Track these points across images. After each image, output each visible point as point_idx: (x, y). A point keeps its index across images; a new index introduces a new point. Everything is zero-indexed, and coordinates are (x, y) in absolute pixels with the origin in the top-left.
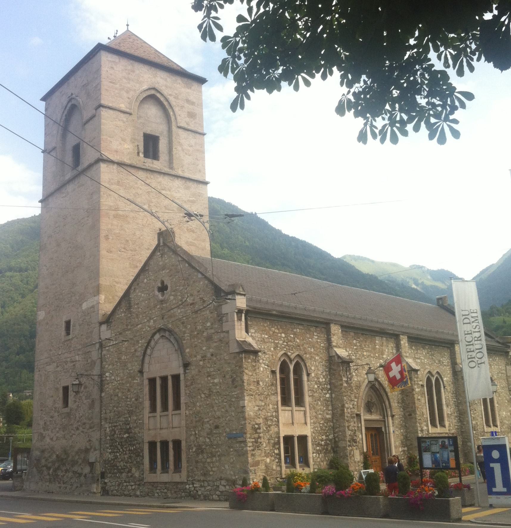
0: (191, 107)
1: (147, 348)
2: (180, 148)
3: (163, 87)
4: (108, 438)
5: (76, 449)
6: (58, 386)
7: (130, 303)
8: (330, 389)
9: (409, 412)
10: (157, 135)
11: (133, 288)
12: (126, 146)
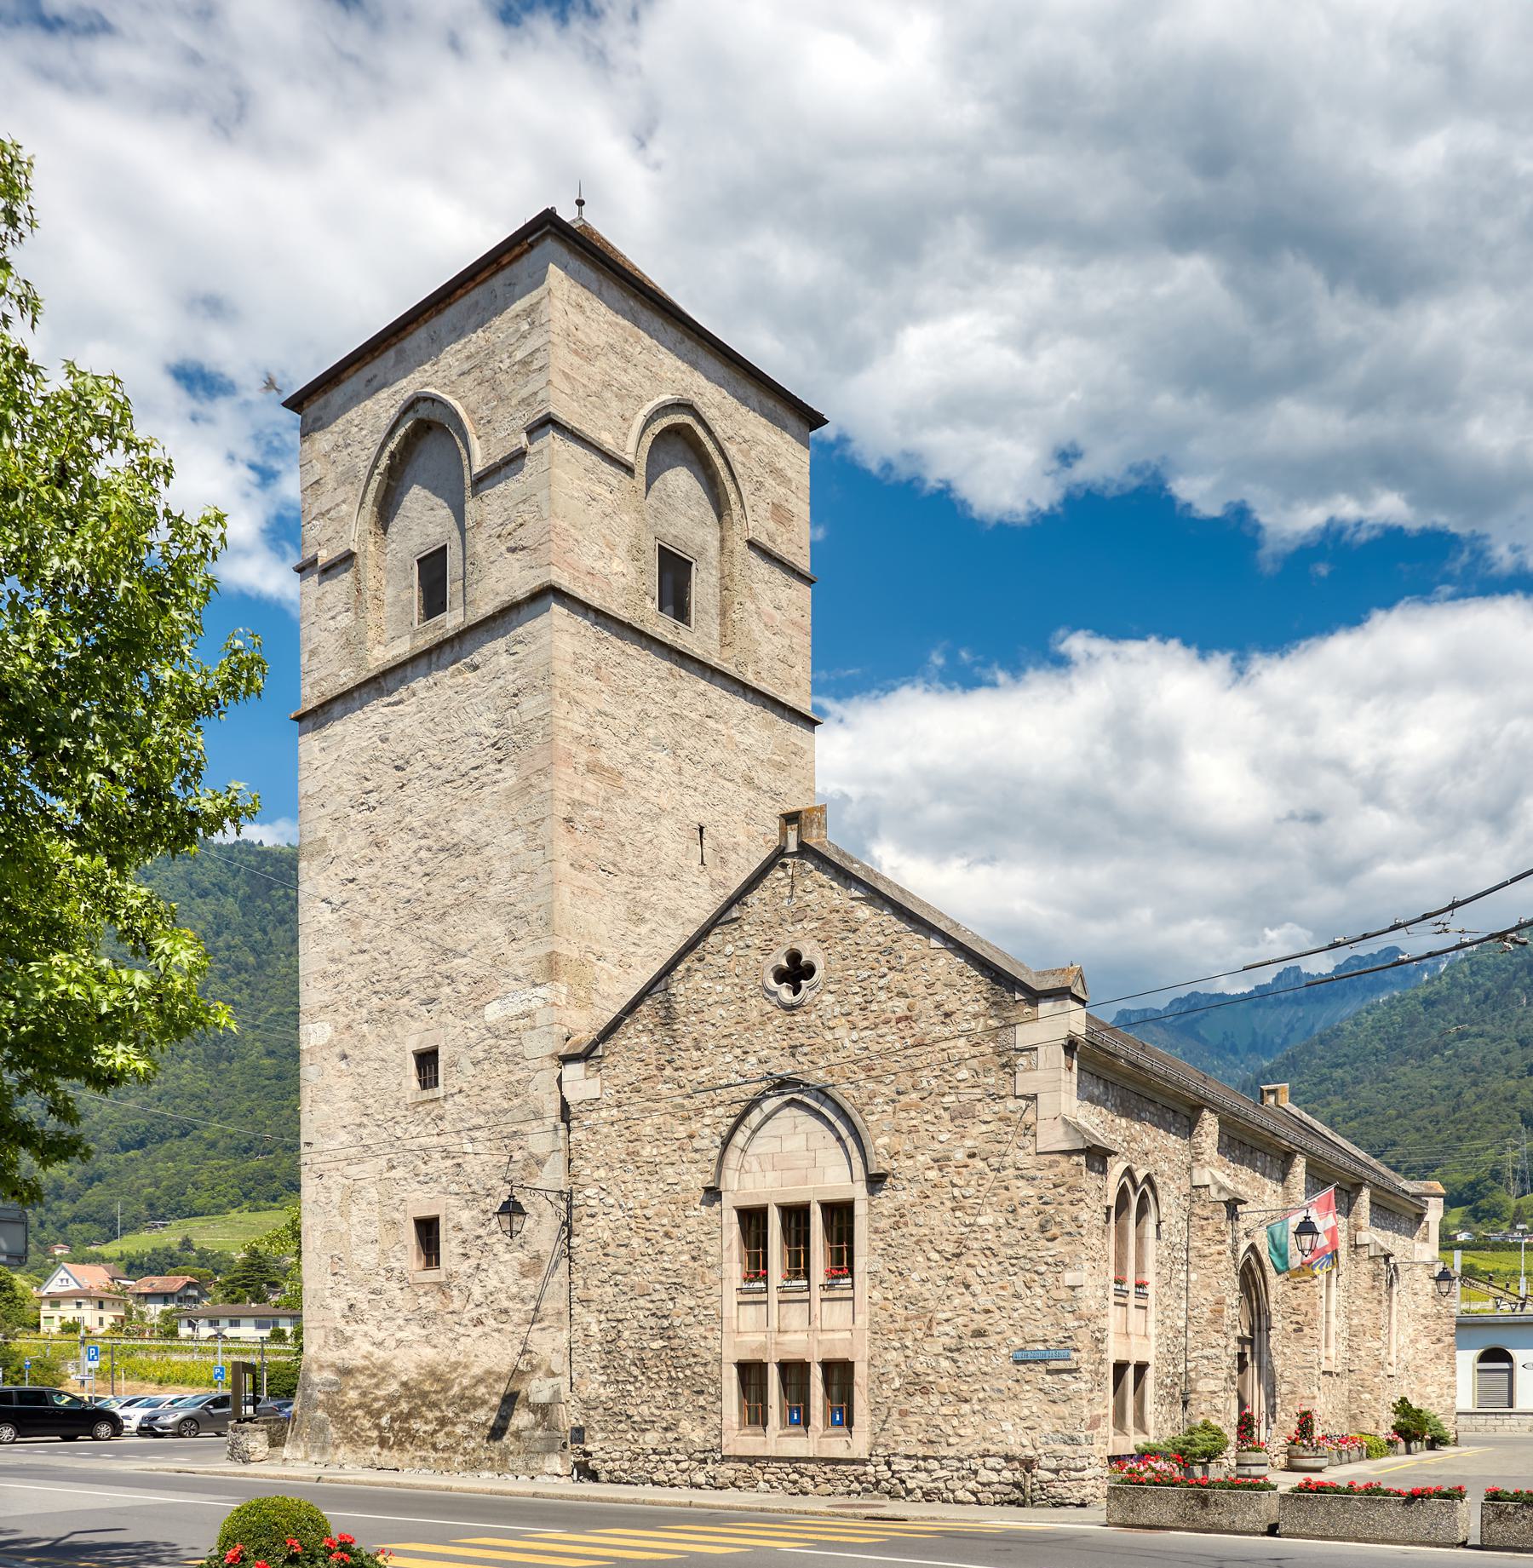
0: (782, 490)
1: (734, 1129)
4: (596, 1347)
5: (477, 1370)
6: (397, 1216)
12: (617, 566)
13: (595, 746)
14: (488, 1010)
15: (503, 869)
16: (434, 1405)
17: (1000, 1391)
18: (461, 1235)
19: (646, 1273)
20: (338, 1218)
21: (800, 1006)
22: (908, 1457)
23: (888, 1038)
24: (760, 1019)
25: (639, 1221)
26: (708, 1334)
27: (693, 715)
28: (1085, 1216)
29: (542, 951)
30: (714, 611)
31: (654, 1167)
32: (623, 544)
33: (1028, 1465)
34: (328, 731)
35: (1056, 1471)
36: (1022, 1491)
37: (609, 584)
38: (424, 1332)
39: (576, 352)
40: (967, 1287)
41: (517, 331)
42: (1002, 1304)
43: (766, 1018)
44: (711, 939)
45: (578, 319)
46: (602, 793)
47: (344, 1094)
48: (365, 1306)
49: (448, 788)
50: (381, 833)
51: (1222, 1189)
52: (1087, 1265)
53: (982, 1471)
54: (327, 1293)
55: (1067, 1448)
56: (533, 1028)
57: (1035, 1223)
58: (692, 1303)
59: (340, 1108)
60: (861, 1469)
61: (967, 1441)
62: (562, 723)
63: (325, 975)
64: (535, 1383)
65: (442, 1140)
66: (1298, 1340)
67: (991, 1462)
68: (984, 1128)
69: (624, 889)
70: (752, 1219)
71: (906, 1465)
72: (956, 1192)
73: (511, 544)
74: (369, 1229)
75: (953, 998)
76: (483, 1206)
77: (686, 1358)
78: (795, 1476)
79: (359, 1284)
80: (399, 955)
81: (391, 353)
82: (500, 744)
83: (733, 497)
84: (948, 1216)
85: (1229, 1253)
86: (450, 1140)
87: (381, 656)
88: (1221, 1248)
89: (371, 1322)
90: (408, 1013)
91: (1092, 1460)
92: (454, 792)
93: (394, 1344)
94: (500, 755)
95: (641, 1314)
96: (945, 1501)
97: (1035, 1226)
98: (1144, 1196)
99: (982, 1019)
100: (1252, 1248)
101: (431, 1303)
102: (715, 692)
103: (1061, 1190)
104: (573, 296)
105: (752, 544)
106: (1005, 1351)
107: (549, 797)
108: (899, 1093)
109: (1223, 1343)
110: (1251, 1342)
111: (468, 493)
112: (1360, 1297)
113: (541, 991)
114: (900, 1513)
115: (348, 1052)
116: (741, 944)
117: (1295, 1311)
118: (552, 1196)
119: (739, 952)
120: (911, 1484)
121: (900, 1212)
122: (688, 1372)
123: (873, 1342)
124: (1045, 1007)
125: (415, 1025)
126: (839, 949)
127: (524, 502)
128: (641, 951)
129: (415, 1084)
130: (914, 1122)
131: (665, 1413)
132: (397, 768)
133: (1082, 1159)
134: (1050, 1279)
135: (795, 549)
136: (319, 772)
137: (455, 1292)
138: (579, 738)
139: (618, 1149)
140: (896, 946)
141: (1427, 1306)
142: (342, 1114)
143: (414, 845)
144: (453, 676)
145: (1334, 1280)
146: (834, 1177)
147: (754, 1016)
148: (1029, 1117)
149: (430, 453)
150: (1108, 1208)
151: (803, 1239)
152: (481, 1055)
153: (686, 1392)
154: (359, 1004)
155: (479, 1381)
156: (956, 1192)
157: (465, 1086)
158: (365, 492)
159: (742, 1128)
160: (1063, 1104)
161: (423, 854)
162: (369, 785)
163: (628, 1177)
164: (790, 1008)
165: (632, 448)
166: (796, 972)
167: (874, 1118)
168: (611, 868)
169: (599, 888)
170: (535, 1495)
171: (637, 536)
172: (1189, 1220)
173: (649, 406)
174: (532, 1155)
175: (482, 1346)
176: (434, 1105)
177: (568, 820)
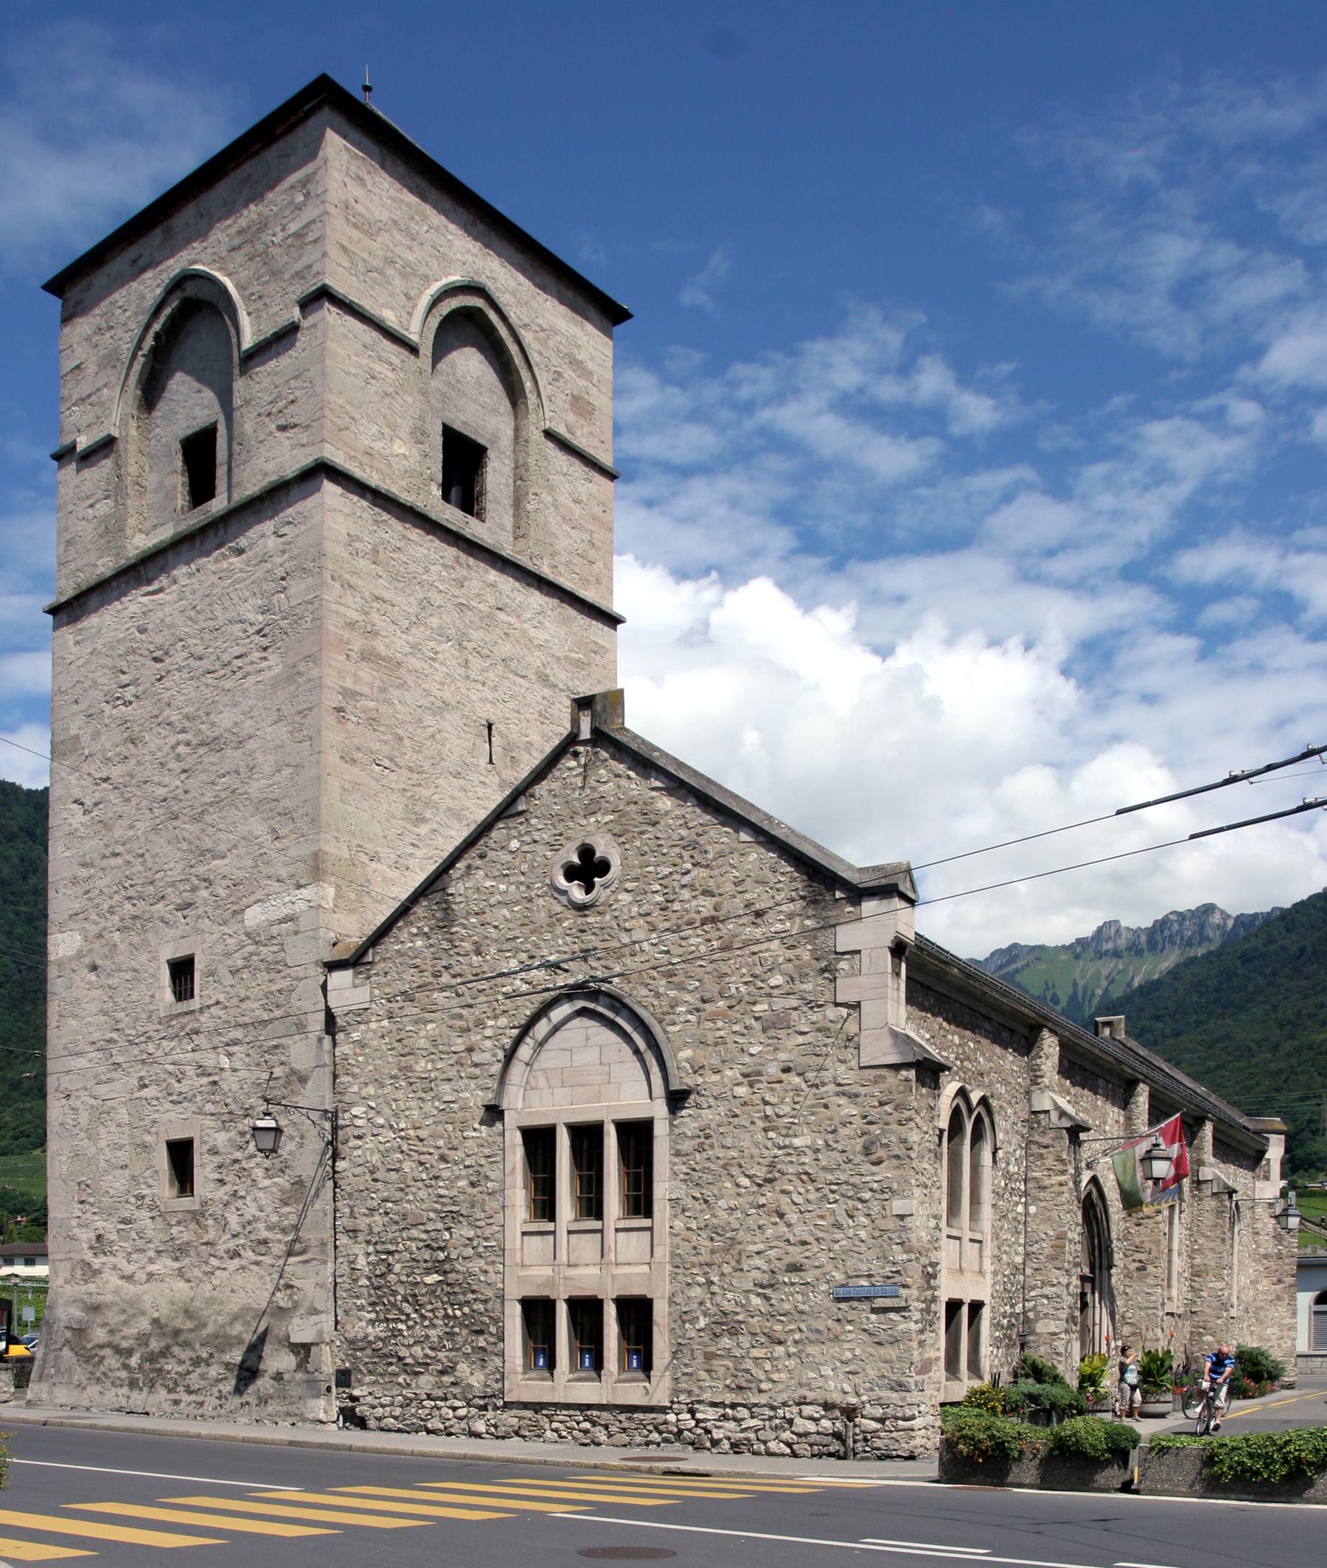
0: (582, 383)
1: (518, 1041)
2: (550, 499)
3: (507, 296)
4: (364, 1282)
6: (148, 1138)
7: (447, 910)
8: (1026, 1194)
9: (1140, 1261)
10: (482, 441)
11: (461, 865)
12: (398, 448)
13: (372, 633)
14: (249, 914)
15: (266, 762)
16: (186, 1345)
17: (818, 1331)
18: (217, 1159)
19: (420, 1202)
20: (86, 1141)
21: (592, 906)
22: (714, 1405)
23: (692, 941)
24: (548, 920)
25: (412, 1143)
26: (490, 1268)
27: (481, 606)
28: (914, 1137)
29: (307, 850)
30: (508, 502)
31: (428, 1085)
32: (405, 426)
33: (850, 1413)
34: (80, 625)
35: (882, 1420)
36: (844, 1442)
37: (390, 466)
38: (177, 1265)
39: (355, 226)
40: (781, 1216)
41: (292, 202)
42: (821, 1235)
43: (555, 919)
44: (495, 834)
45: (357, 191)
46: (377, 683)
47: (93, 1008)
48: (114, 1237)
49: (209, 679)
50: (137, 729)
51: (1063, 1114)
52: (918, 1192)
53: (798, 1421)
54: (74, 1223)
55: (895, 1395)
56: (296, 933)
57: (858, 1144)
58: (471, 1234)
59: (90, 1024)
60: (661, 1417)
61: (781, 1387)
62: (334, 607)
63: (75, 881)
64: (296, 1321)
65: (197, 1056)
66: (1141, 1279)
67: (808, 1410)
68: (800, 1039)
69: (402, 786)
70: (538, 1142)
71: (709, 1414)
72: (769, 1111)
73: (282, 422)
74: (119, 1154)
75: (764, 896)
76: (240, 1127)
77: (464, 1294)
78: (587, 1425)
79: (107, 1212)
80: (154, 857)
81: (158, 232)
82: (266, 631)
83: (528, 385)
84: (759, 1137)
85: (1071, 1184)
86: (209, 1060)
87: (140, 543)
88: (1063, 1178)
89: (121, 1254)
90: (162, 920)
91: (922, 1408)
92: (216, 683)
93: (144, 1277)
94: (265, 642)
95: (414, 1245)
96: (755, 1453)
97: (859, 1148)
98: (979, 1120)
99: (798, 920)
100: (1094, 1180)
101: (183, 1234)
102: (507, 584)
103: (888, 1108)
104: (353, 168)
105: (549, 435)
106: (824, 1287)
107: (318, 684)
108: (704, 1001)
109: (1064, 1280)
110: (1092, 1280)
111: (236, 371)
112: (1204, 1235)
113: (305, 893)
114: (702, 1469)
115: (99, 962)
116: (527, 839)
117: (1138, 1249)
118: (315, 1116)
119: (525, 848)
120: (717, 1434)
121: (705, 1133)
122: (466, 1310)
123: (674, 1276)
124: (869, 906)
125: (172, 932)
126: (638, 843)
127: (296, 378)
128: (419, 853)
129: (169, 995)
130: (721, 1033)
131: (441, 1355)
132: (156, 660)
133: (912, 1074)
134: (875, 1208)
135: (596, 443)
136: (73, 667)
137: (210, 1222)
138: (351, 625)
139: (390, 1063)
140: (701, 840)
141: (1269, 1246)
142: (91, 1029)
143: (172, 740)
144: (217, 561)
145: (1176, 1217)
146: (625, 1093)
147: (542, 917)
148: (851, 1027)
149: (198, 340)
150: (941, 1131)
151: (594, 1165)
152: (240, 963)
153: (465, 1332)
154: (111, 911)
155: (235, 1318)
156: (769, 1111)
157: (222, 997)
158: (127, 375)
159: (528, 1040)
160: (890, 1012)
161: (182, 749)
162: (125, 679)
163: (400, 1095)
164: (581, 908)
165: (418, 328)
166: (588, 868)
167: (677, 1028)
168: (387, 763)
169: (373, 783)
170: (291, 1443)
171: (422, 418)
172: (1027, 1148)
173: (435, 287)
174: (293, 1072)
175: (239, 1279)
176: (187, 1019)
177: (339, 710)
